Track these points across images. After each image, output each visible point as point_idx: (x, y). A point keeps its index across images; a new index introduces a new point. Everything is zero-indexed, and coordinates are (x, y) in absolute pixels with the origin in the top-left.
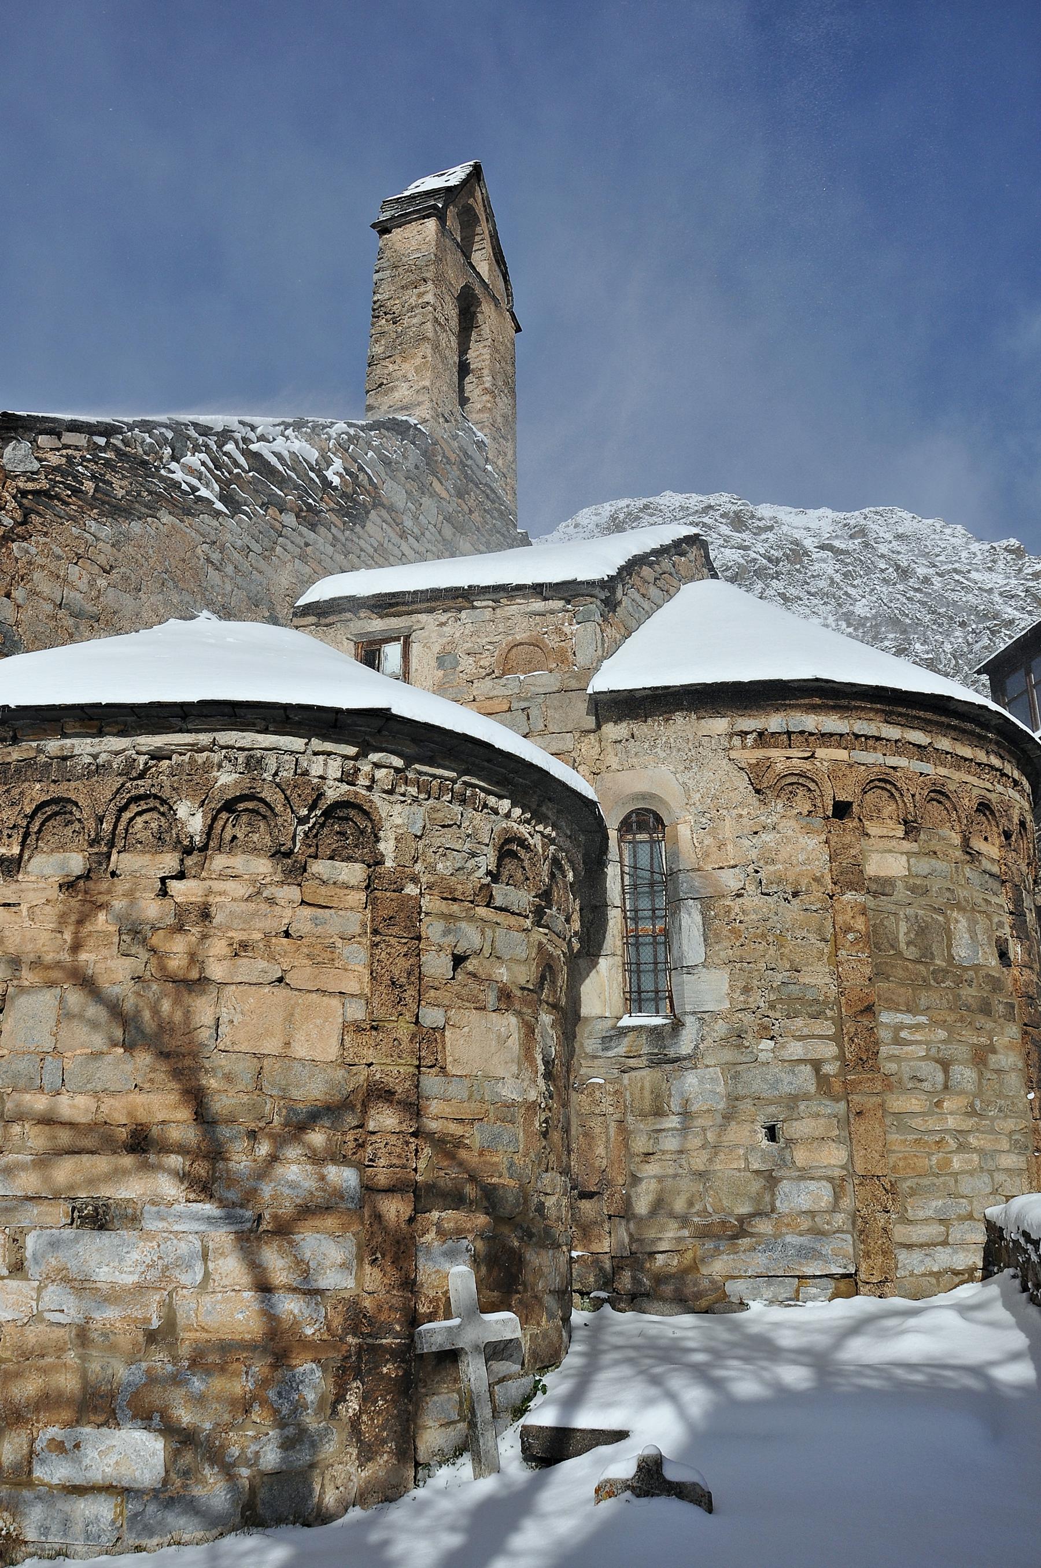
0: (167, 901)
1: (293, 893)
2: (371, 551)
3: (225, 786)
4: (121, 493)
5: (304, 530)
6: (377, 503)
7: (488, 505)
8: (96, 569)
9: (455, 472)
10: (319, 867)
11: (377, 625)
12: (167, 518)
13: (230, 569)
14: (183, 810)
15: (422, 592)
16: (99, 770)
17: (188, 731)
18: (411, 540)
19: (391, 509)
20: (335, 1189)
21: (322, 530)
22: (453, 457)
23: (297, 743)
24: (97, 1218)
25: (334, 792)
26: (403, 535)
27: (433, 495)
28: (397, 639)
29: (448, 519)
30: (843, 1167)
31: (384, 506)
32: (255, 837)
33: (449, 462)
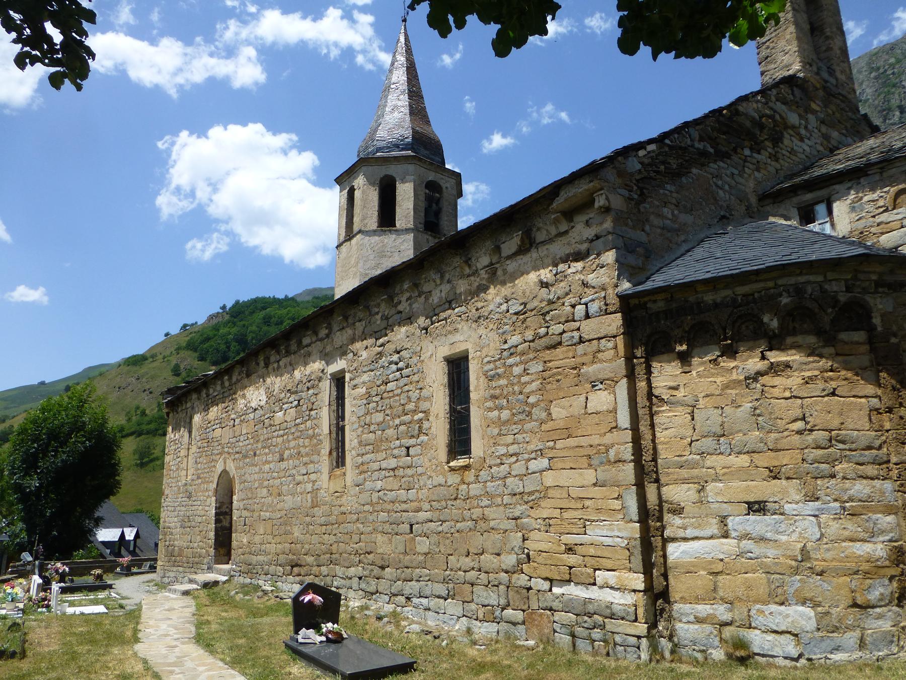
0: (766, 362)
1: (831, 350)
2: (788, 154)
3: (786, 304)
4: (675, 166)
5: (755, 155)
6: (786, 127)
7: (843, 105)
8: (673, 207)
9: (821, 93)
10: (843, 336)
11: (809, 197)
12: (694, 171)
13: (727, 187)
14: (766, 319)
15: (696, 122)
16: (716, 305)
17: (760, 281)
18: (806, 141)
19: (793, 127)
20: (117, 465)
21: (762, 151)
22: (818, 85)
23: (820, 278)
24: (757, 507)
25: (843, 298)
26: (802, 140)
27: (814, 112)
28: (822, 201)
29: (823, 122)
30: (657, 413)
31: (789, 127)
32: (805, 326)
33: (817, 89)
